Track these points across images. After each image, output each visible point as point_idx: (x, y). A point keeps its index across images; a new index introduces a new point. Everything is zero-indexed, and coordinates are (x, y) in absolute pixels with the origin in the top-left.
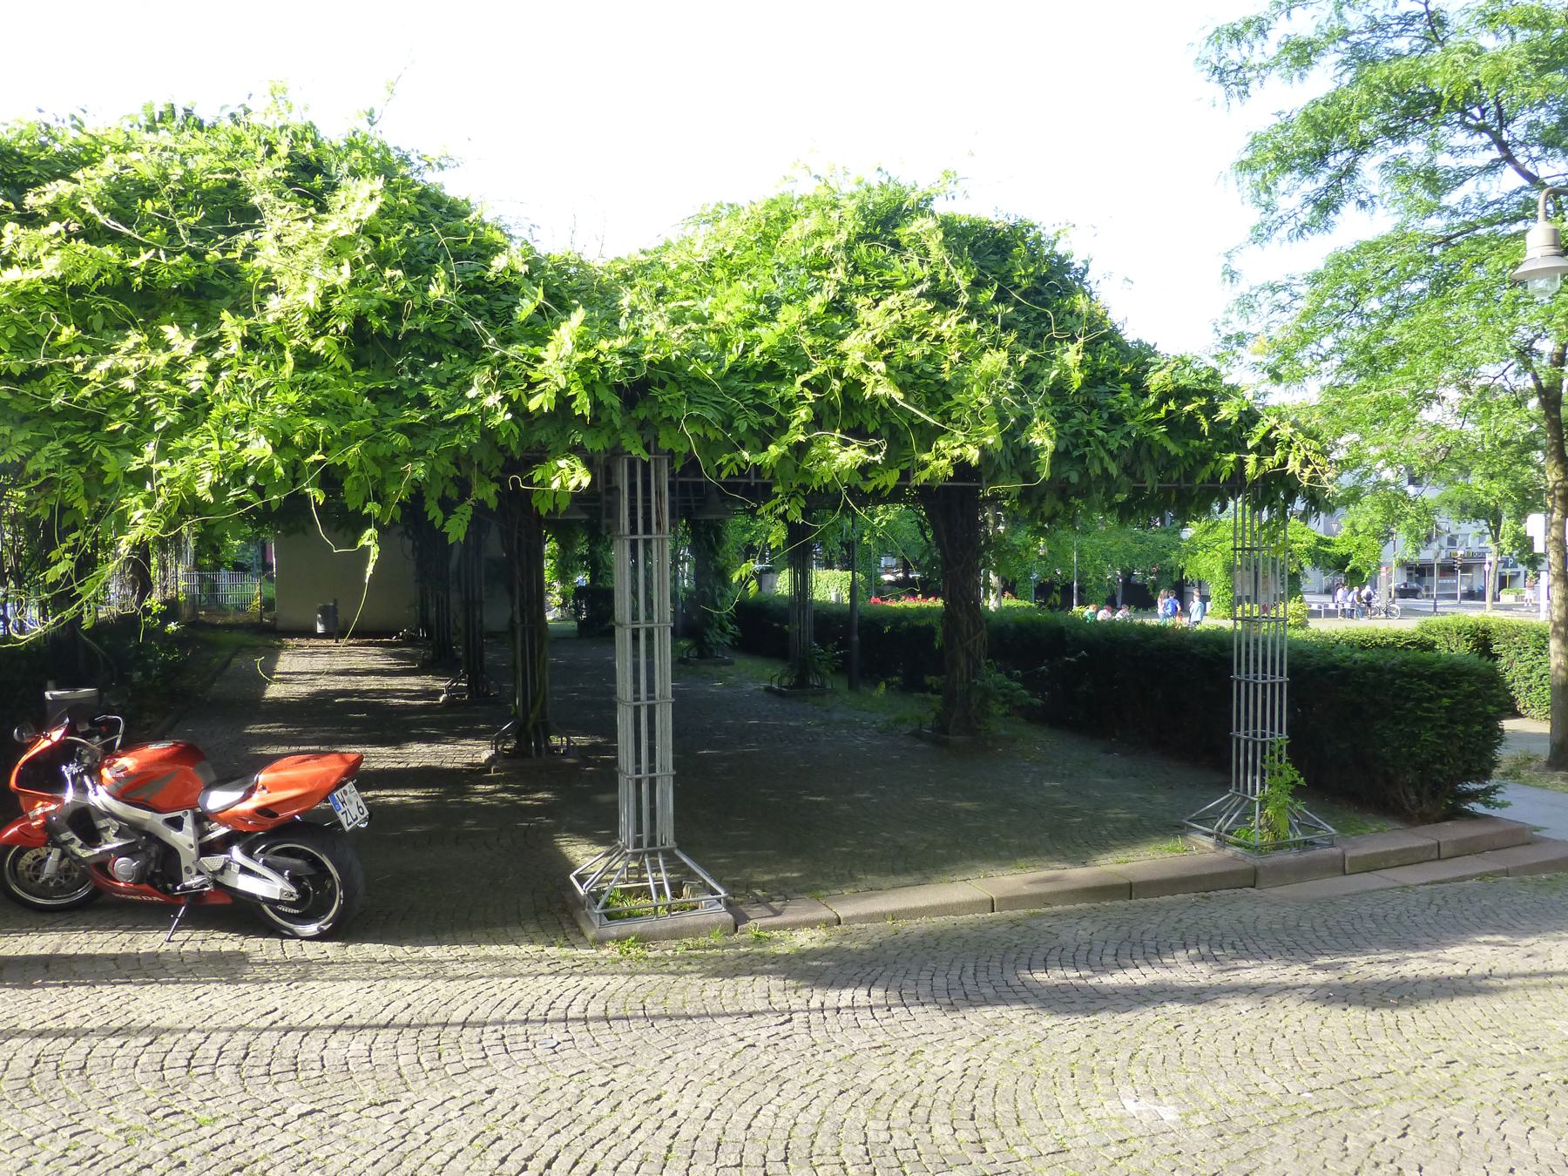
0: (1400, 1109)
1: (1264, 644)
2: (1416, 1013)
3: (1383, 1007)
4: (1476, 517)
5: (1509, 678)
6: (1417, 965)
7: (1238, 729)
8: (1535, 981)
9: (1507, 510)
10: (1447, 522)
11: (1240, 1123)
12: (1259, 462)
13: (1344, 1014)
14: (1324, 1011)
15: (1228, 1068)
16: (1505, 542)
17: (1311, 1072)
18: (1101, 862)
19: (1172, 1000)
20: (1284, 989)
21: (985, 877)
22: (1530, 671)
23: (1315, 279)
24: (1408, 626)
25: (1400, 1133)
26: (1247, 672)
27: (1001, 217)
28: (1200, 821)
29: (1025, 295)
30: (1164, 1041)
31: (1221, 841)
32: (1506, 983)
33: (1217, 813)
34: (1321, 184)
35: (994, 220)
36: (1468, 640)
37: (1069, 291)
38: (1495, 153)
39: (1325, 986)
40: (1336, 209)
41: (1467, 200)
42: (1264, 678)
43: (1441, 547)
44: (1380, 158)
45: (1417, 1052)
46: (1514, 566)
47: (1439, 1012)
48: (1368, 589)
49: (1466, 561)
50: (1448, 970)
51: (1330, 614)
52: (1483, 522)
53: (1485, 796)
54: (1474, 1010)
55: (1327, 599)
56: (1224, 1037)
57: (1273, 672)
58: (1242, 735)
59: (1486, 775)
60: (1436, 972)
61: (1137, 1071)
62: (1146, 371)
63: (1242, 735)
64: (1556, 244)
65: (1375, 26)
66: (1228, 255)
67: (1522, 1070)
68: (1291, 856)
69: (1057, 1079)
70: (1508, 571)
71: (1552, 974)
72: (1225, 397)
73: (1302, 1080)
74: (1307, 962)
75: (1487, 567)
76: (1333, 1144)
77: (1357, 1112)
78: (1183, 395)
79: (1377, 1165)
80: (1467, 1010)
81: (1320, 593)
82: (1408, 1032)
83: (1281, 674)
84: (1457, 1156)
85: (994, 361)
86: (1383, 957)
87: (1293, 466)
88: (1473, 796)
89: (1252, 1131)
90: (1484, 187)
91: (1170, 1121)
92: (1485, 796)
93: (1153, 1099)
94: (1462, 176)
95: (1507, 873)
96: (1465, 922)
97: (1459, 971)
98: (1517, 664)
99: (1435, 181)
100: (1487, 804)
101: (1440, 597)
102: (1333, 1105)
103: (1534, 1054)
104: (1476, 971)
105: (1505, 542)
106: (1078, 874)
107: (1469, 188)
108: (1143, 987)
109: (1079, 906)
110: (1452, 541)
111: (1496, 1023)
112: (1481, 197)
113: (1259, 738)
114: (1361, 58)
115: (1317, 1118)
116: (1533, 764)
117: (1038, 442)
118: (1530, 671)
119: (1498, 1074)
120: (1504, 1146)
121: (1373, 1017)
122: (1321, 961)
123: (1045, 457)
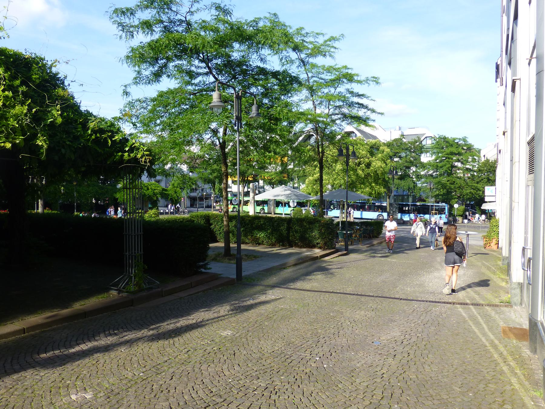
0: (171, 370)
1: (138, 222)
2: (180, 338)
3: (170, 338)
4: (209, 183)
5: (215, 231)
6: (183, 322)
7: (126, 252)
8: (215, 320)
9: (217, 181)
10: (200, 184)
11: (117, 391)
12: (129, 155)
13: (157, 343)
14: (150, 344)
15: (114, 372)
16: (217, 190)
17: (143, 366)
18: (74, 306)
19: (96, 353)
20: (139, 339)
21: (22, 320)
22: (220, 228)
23: (153, 100)
24: (186, 216)
25: (171, 378)
26: (129, 232)
27: (28, 53)
28: (114, 285)
29: (38, 86)
30: (91, 368)
31: (120, 291)
32: (207, 322)
33: (119, 282)
34: (156, 69)
35: (25, 54)
36: (203, 220)
37: (56, 86)
38: (207, 70)
39: (153, 335)
40: (161, 76)
41: (200, 81)
42: (135, 233)
43: (200, 192)
44: (173, 64)
45: (179, 350)
46: (219, 198)
47: (187, 336)
48: (178, 205)
49: (207, 196)
50: (191, 322)
51: (167, 213)
52: (210, 184)
53: (204, 267)
54: (197, 333)
55: (165, 209)
56: (115, 361)
57: (138, 231)
58: (127, 253)
59: (205, 260)
60: (187, 323)
61: (78, 383)
62: (88, 122)
63: (127, 253)
64: (220, 98)
65: (171, 22)
66: (125, 86)
67: (208, 348)
68: (144, 294)
69: (43, 396)
70: (218, 199)
71: (219, 317)
72: (117, 133)
73: (140, 370)
74: (147, 328)
75: (212, 198)
76: (148, 389)
77: (157, 376)
78: (101, 131)
79: (162, 391)
80: (195, 333)
81: (164, 207)
82: (177, 345)
83: (140, 231)
84: (187, 381)
85: (19, 109)
86: (172, 322)
87: (139, 156)
88: (202, 267)
89: (120, 393)
90: (205, 79)
91: (89, 398)
92: (204, 267)
93: (84, 392)
94: (199, 74)
95: (210, 289)
96: (197, 306)
97: (194, 321)
98: (217, 226)
99: (192, 75)
100: (205, 269)
101: (199, 207)
102: (150, 375)
103: (212, 342)
104: (199, 320)
105: (217, 190)
106: (65, 312)
107: (200, 78)
108: (86, 350)
109: (59, 326)
110: (202, 190)
111: (203, 335)
112: (204, 82)
113: (134, 254)
114: (166, 30)
115: (144, 382)
116: (220, 256)
117: (40, 144)
118: (220, 228)
119: (202, 351)
120: (201, 373)
121: (166, 342)
122: (152, 327)
123: (44, 151)
